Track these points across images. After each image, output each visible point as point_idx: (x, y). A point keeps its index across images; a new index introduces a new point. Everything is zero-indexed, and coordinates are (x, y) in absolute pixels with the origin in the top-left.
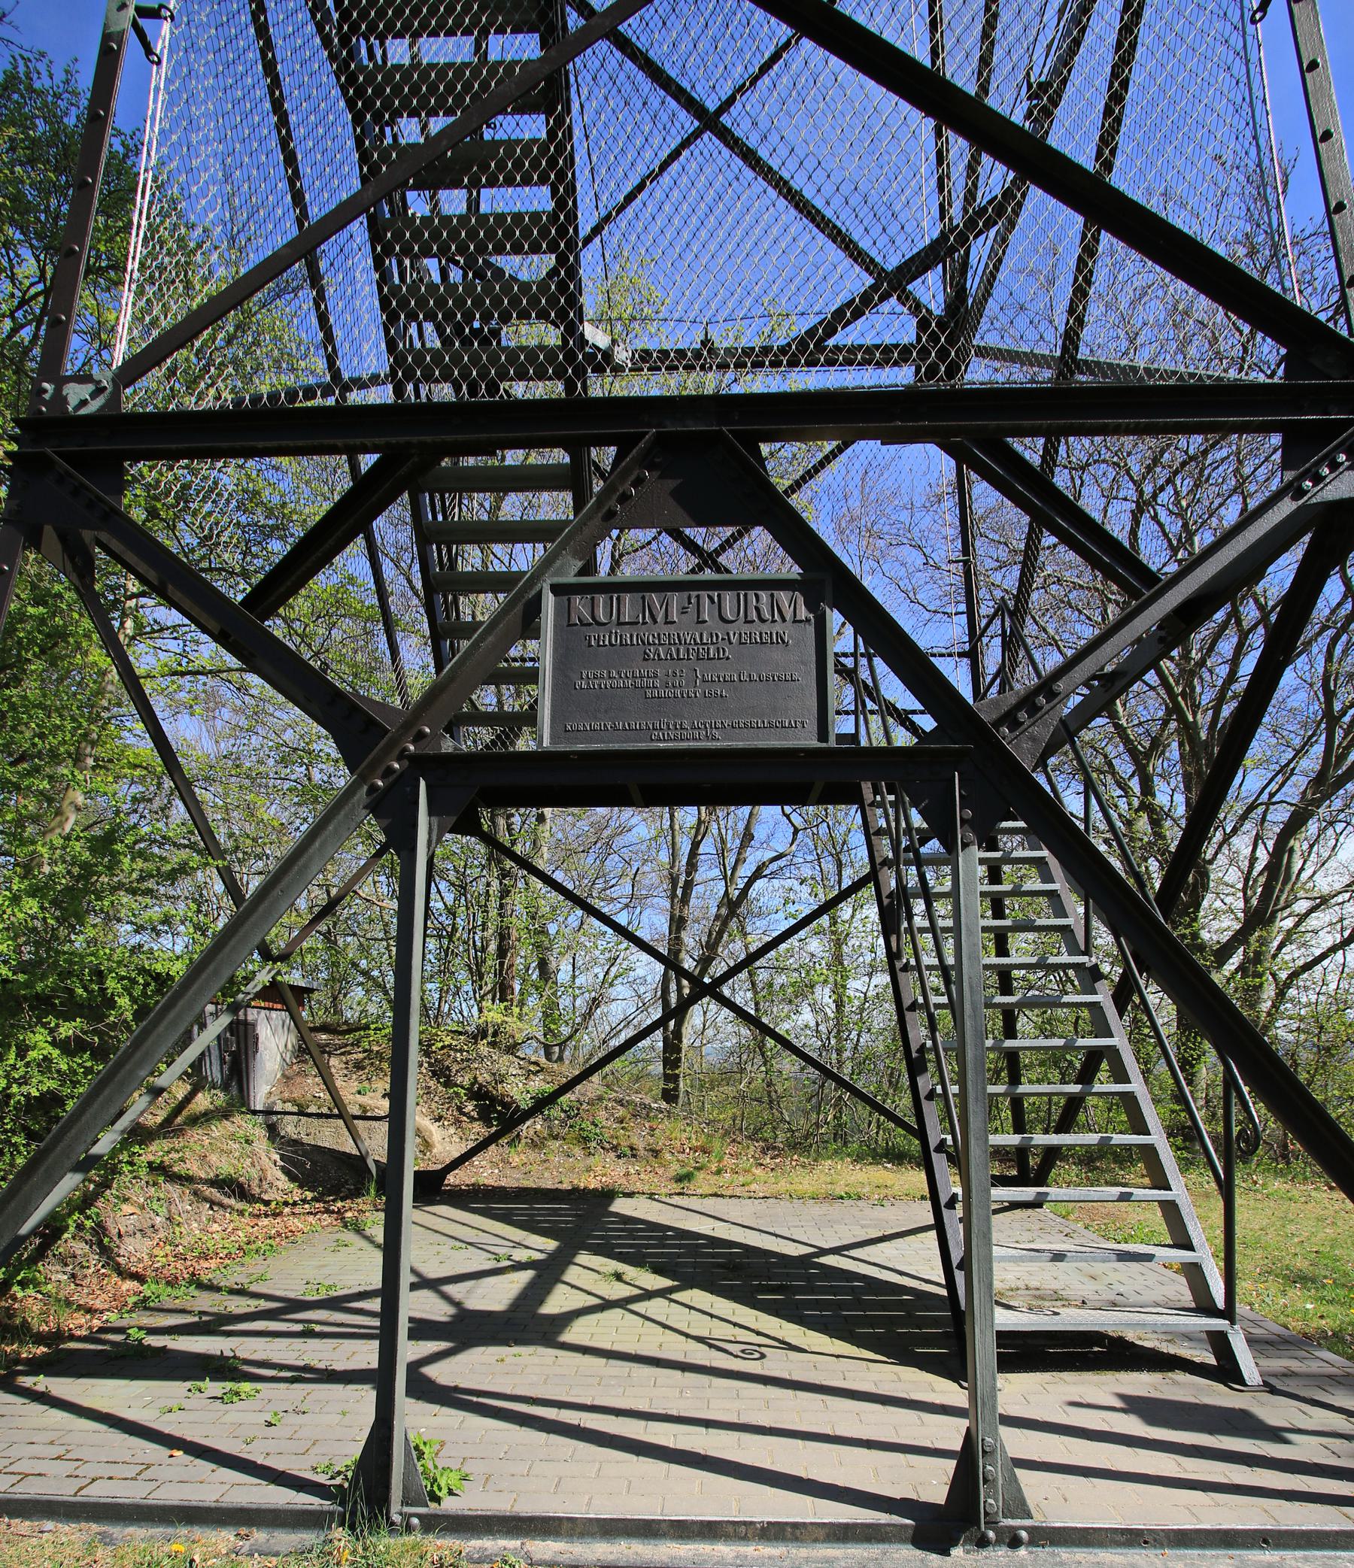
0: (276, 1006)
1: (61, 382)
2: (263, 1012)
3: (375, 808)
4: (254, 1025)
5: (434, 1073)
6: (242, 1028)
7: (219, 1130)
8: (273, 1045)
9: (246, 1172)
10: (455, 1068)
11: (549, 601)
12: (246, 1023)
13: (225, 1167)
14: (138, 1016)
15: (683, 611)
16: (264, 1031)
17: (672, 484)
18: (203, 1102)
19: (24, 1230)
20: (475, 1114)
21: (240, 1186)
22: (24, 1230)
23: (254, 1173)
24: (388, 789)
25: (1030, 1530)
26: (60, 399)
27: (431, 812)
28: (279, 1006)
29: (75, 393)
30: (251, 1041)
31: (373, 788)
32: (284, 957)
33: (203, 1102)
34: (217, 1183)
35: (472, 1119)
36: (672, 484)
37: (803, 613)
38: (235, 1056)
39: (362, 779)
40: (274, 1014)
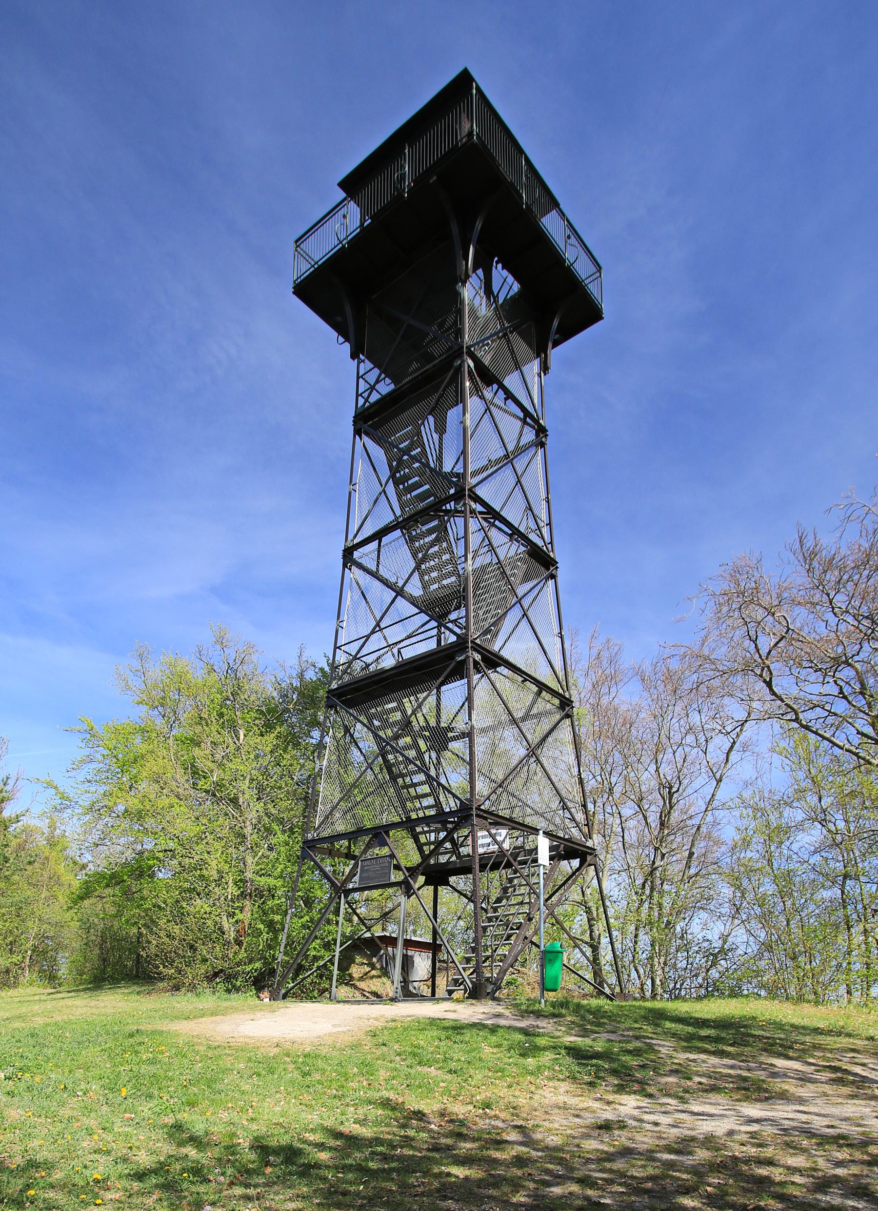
4: (412, 957)
13: (374, 989)
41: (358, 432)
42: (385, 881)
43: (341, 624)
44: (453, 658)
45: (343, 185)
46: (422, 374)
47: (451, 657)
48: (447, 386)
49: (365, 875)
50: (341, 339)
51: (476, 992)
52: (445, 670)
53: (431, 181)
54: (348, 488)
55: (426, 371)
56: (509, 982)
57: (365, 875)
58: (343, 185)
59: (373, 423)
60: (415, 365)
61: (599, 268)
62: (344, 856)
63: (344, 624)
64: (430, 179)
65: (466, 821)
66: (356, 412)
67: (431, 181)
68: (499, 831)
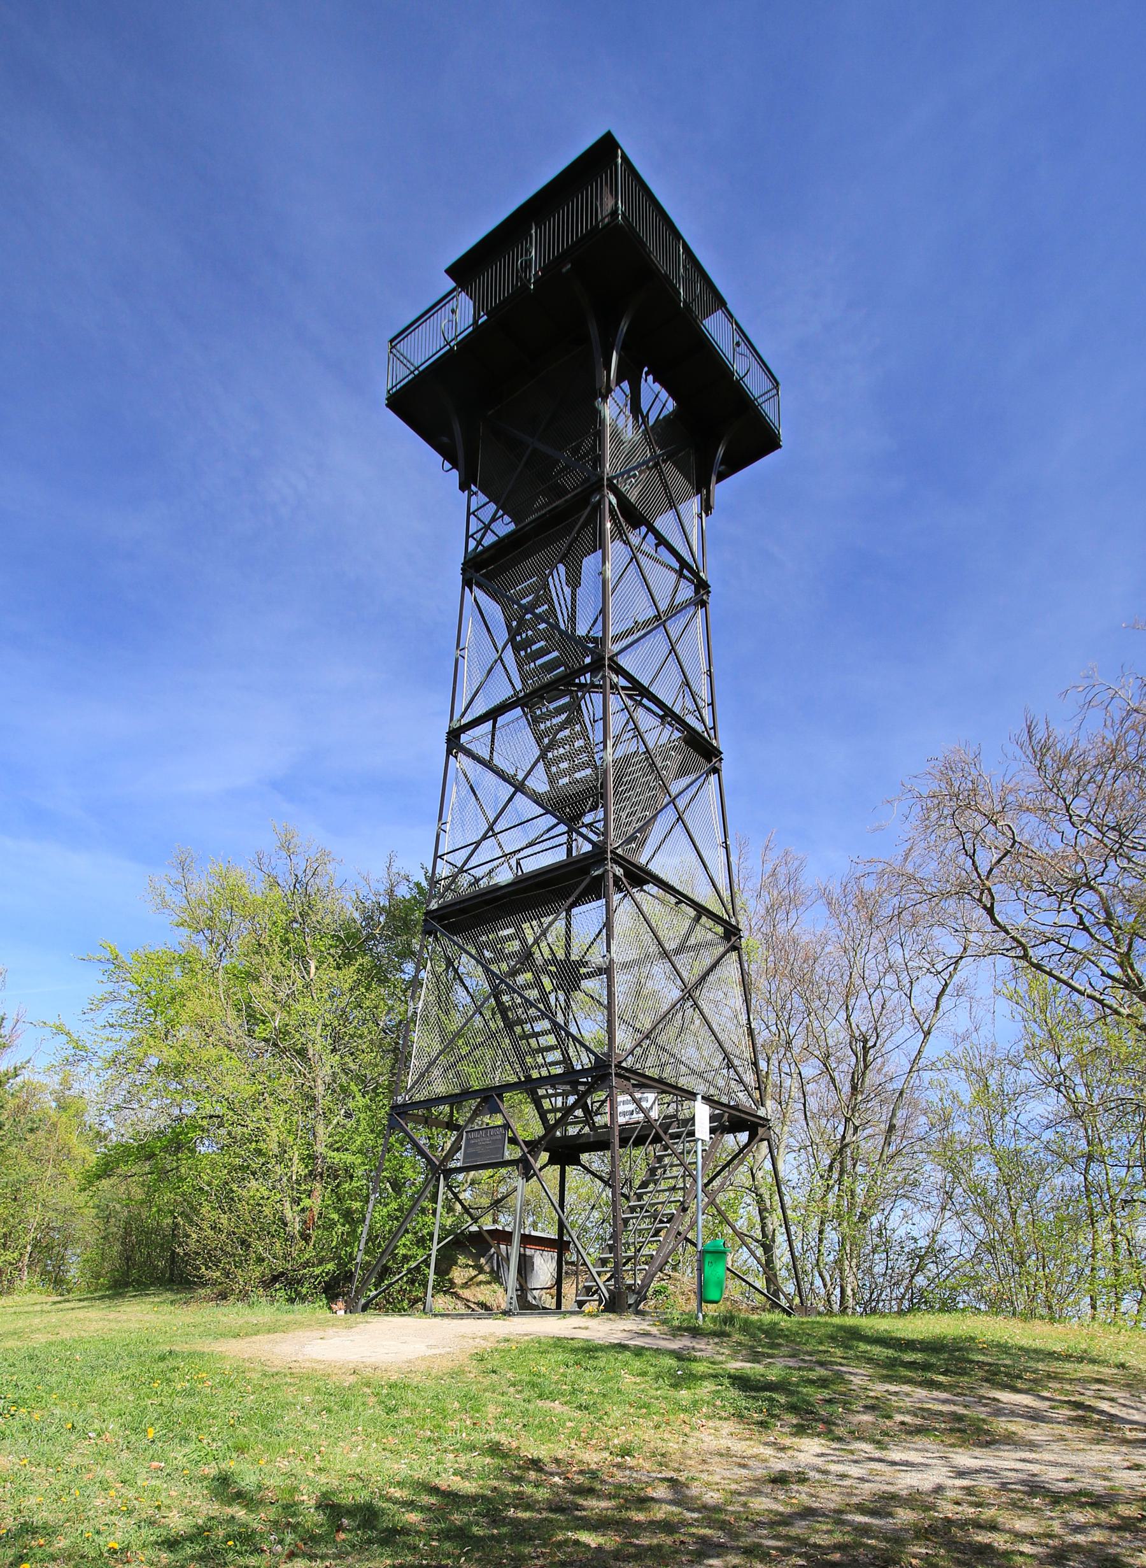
13: (481, 1298)
41: (467, 583)
42: (497, 1158)
45: (452, 271)
46: (550, 511)
48: (582, 528)
49: (471, 1150)
50: (448, 466)
51: (614, 1304)
53: (564, 270)
56: (657, 1291)
57: (471, 1150)
60: (541, 500)
63: (448, 827)
66: (465, 557)
67: (564, 270)
68: (645, 1095)
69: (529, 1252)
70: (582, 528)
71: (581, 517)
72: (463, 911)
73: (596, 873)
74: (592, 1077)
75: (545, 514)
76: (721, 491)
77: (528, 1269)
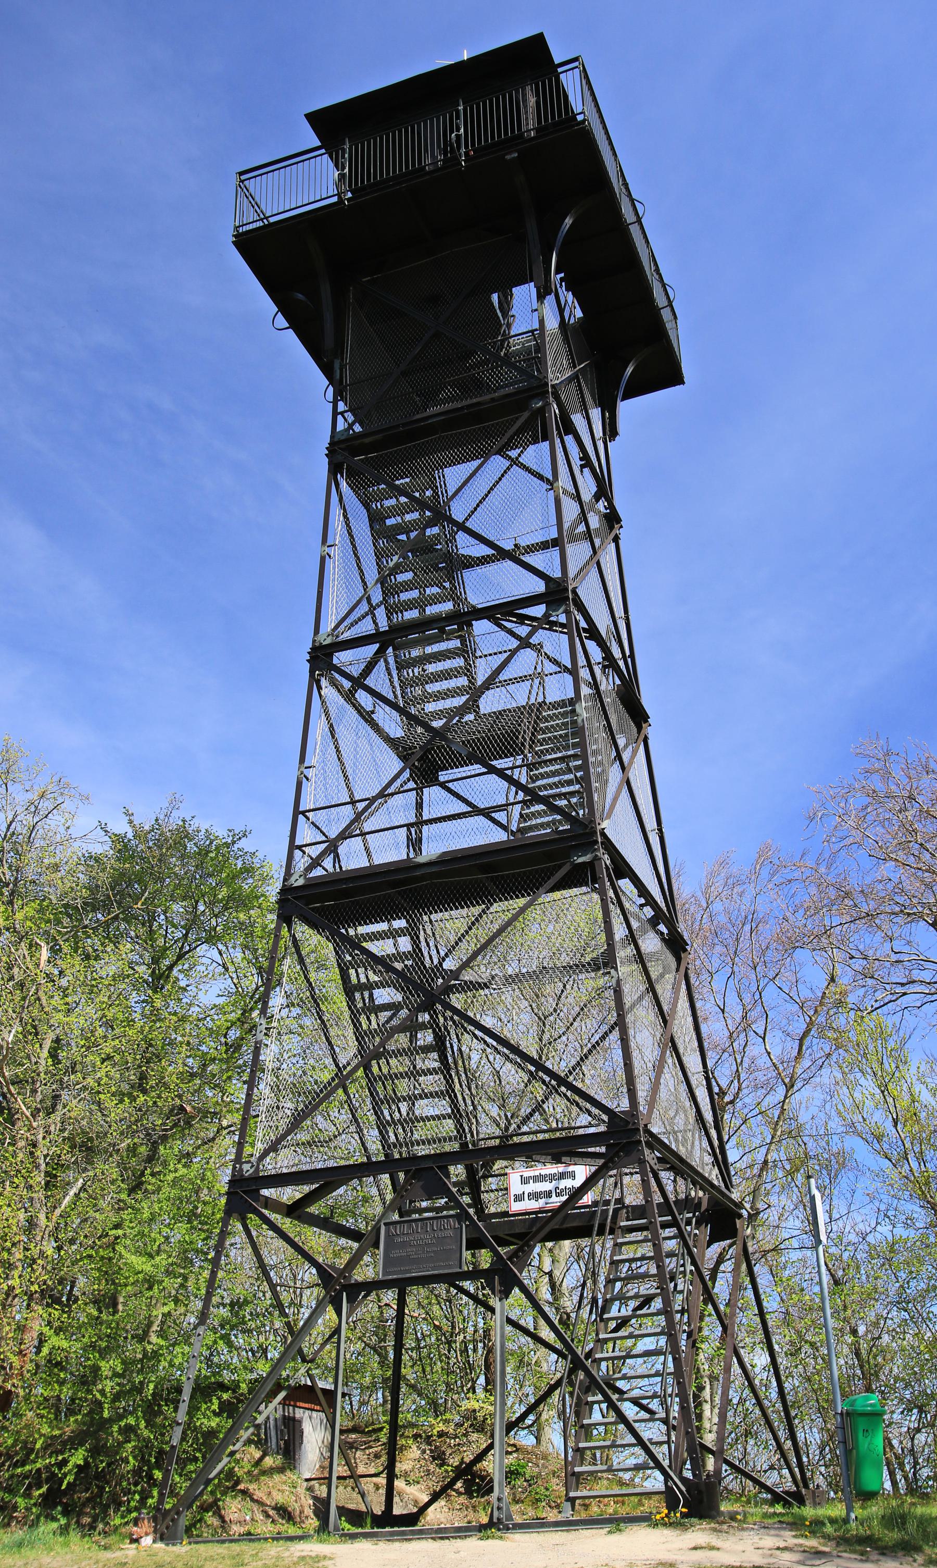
0: (316, 1407)
1: (241, 1163)
2: (307, 1412)
3: (331, 1302)
4: (300, 1422)
5: (434, 1458)
6: (291, 1423)
7: (277, 1478)
8: (314, 1440)
9: (294, 1507)
10: (449, 1451)
11: (383, 1228)
12: (294, 1419)
13: (279, 1498)
14: (250, 1392)
15: (422, 1228)
16: (307, 1427)
17: (421, 1183)
18: (269, 1461)
19: (211, 1476)
20: (462, 1490)
21: (289, 1513)
22: (211, 1476)
23: (296, 1506)
24: (335, 1295)
25: (512, 1524)
26: (241, 1170)
27: (348, 1302)
28: (318, 1408)
29: (246, 1167)
30: (297, 1436)
31: (331, 1296)
32: (312, 1361)
33: (269, 1461)
34: (277, 1508)
35: (460, 1494)
36: (421, 1183)
37: (457, 1226)
38: (287, 1443)
39: (327, 1293)
40: (314, 1414)
41: (335, 469)
42: (450, 1267)
43: (306, 772)
44: (569, 857)
45: (317, 119)
46: (468, 406)
47: (566, 854)
48: (517, 433)
49: (395, 1254)
50: (281, 321)
51: (701, 1502)
52: (552, 874)
53: (508, 157)
54: (317, 549)
55: (478, 404)
56: (511, 1472)
57: (395, 1254)
58: (317, 119)
59: (366, 459)
60: (448, 391)
61: (675, 318)
62: (285, 1210)
63: (310, 773)
64: (507, 154)
65: (628, 1154)
66: (332, 437)
67: (508, 157)
68: (571, 1168)
69: (299, 1413)
70: (517, 433)
71: (517, 418)
72: (346, 893)
73: (581, 860)
74: (608, 1147)
75: (462, 408)
76: (627, 409)
77: (297, 1443)
